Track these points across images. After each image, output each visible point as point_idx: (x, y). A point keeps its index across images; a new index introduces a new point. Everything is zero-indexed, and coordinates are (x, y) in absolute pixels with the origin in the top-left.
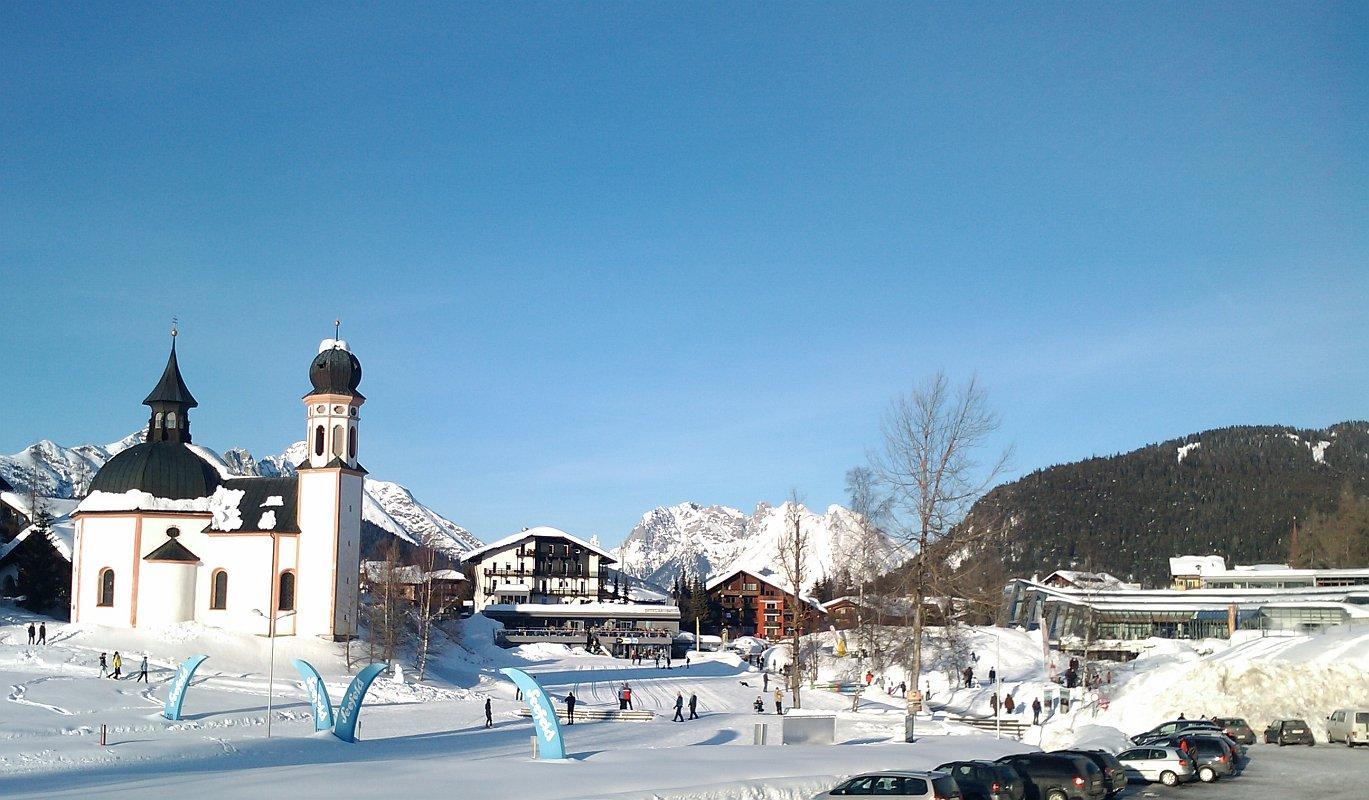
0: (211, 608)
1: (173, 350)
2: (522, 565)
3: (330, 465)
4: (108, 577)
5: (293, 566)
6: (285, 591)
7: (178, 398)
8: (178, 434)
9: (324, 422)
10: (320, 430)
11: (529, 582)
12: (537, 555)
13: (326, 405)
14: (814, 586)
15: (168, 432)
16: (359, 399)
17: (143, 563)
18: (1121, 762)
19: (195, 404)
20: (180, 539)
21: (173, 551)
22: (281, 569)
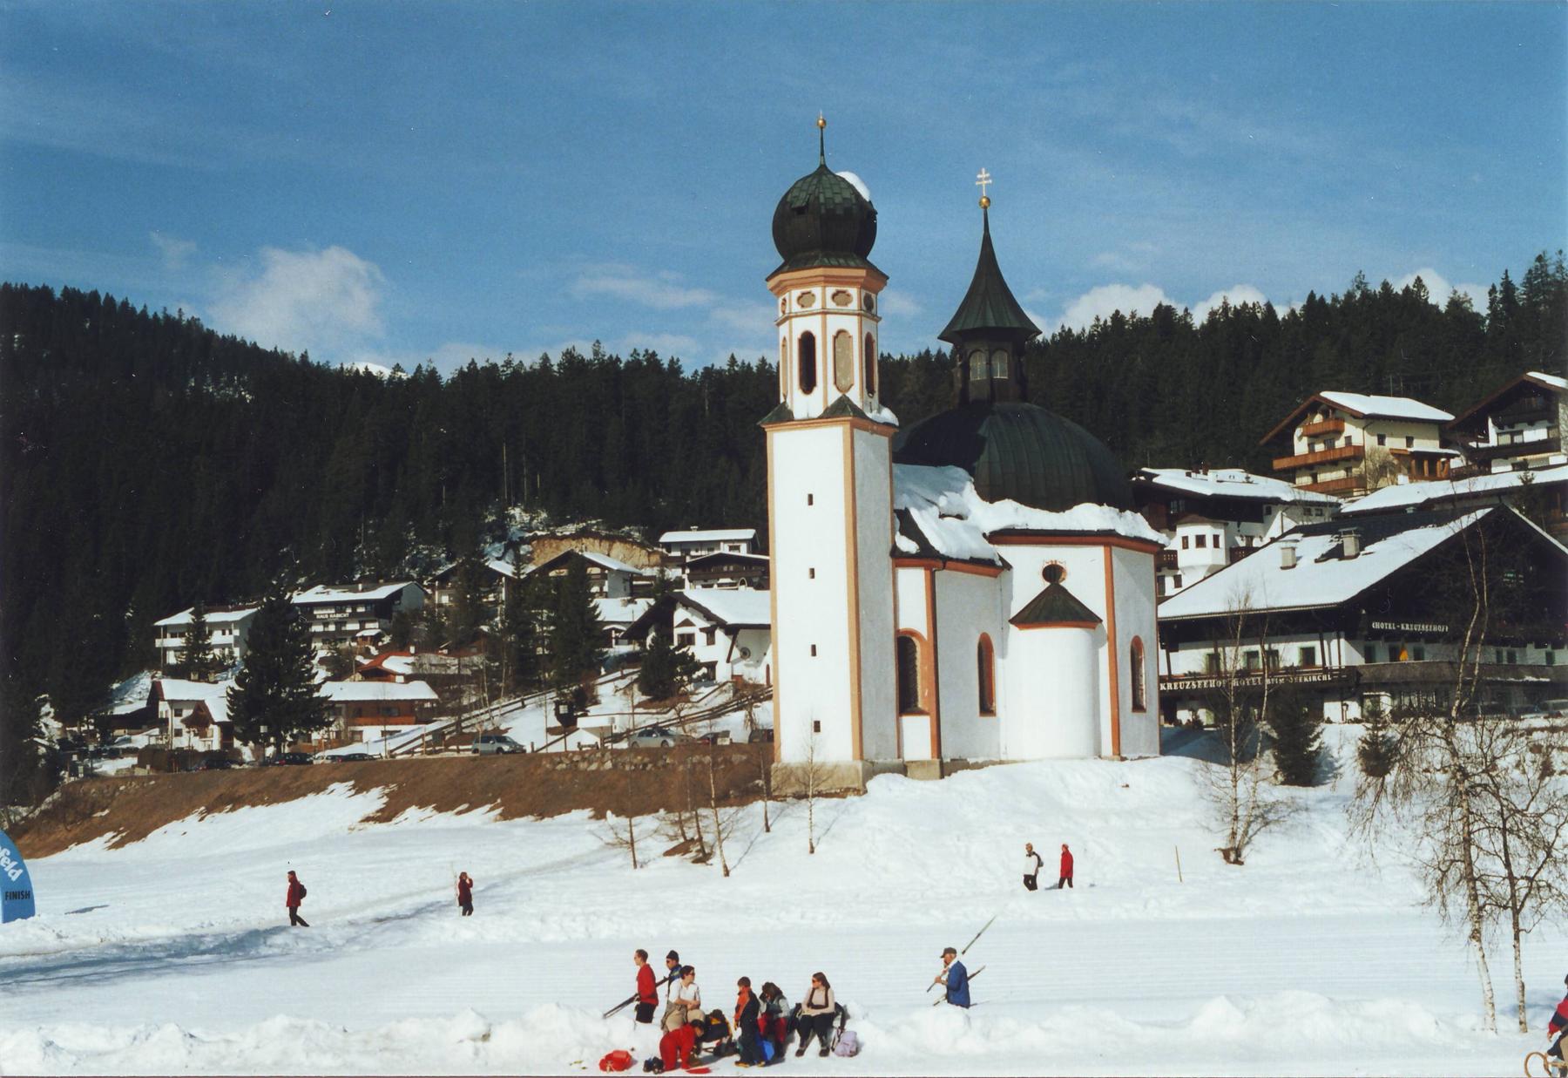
1: (987, 241)
9: (813, 325)
10: (807, 342)
16: (876, 279)
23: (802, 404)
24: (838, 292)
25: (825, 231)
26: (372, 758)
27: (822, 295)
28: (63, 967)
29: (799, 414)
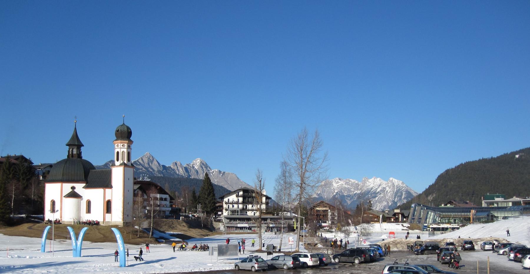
1: (75, 128)
3: (121, 165)
4: (53, 203)
5: (110, 199)
9: (119, 150)
10: (118, 153)
12: (244, 197)
14: (356, 206)
17: (64, 198)
18: (300, 259)
20: (76, 190)
21: (73, 195)
22: (107, 200)
27: (120, 145)
28: (103, 256)
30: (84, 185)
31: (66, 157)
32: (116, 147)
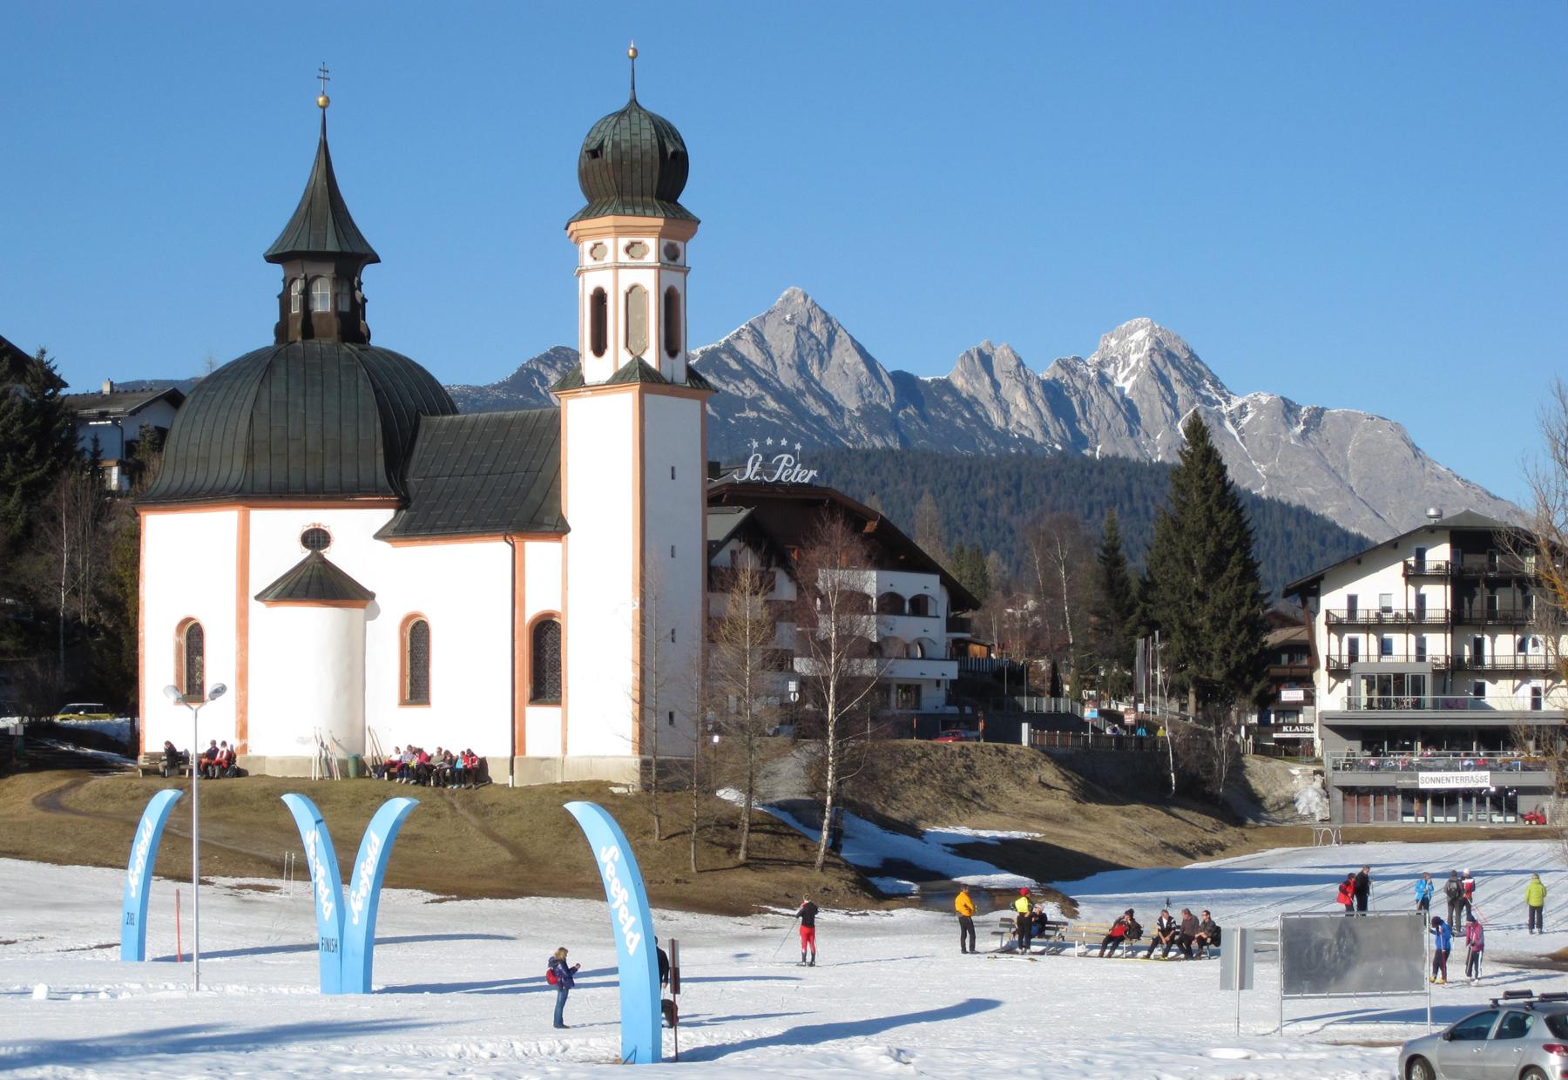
0: (403, 703)
1: (324, 147)
2: (1421, 600)
4: (193, 639)
5: (555, 606)
6: (542, 661)
7: (331, 246)
8: (335, 324)
9: (603, 279)
10: (599, 299)
11: (1438, 646)
12: (1460, 581)
13: (608, 242)
15: (315, 321)
17: (256, 608)
19: (376, 260)
20: (332, 554)
21: (317, 583)
22: (532, 611)
23: (596, 369)
24: (632, 244)
25: (643, 173)
26: (168, 877)
27: (615, 246)
29: (589, 378)
30: (385, 516)
31: (269, 340)
32: (588, 261)
